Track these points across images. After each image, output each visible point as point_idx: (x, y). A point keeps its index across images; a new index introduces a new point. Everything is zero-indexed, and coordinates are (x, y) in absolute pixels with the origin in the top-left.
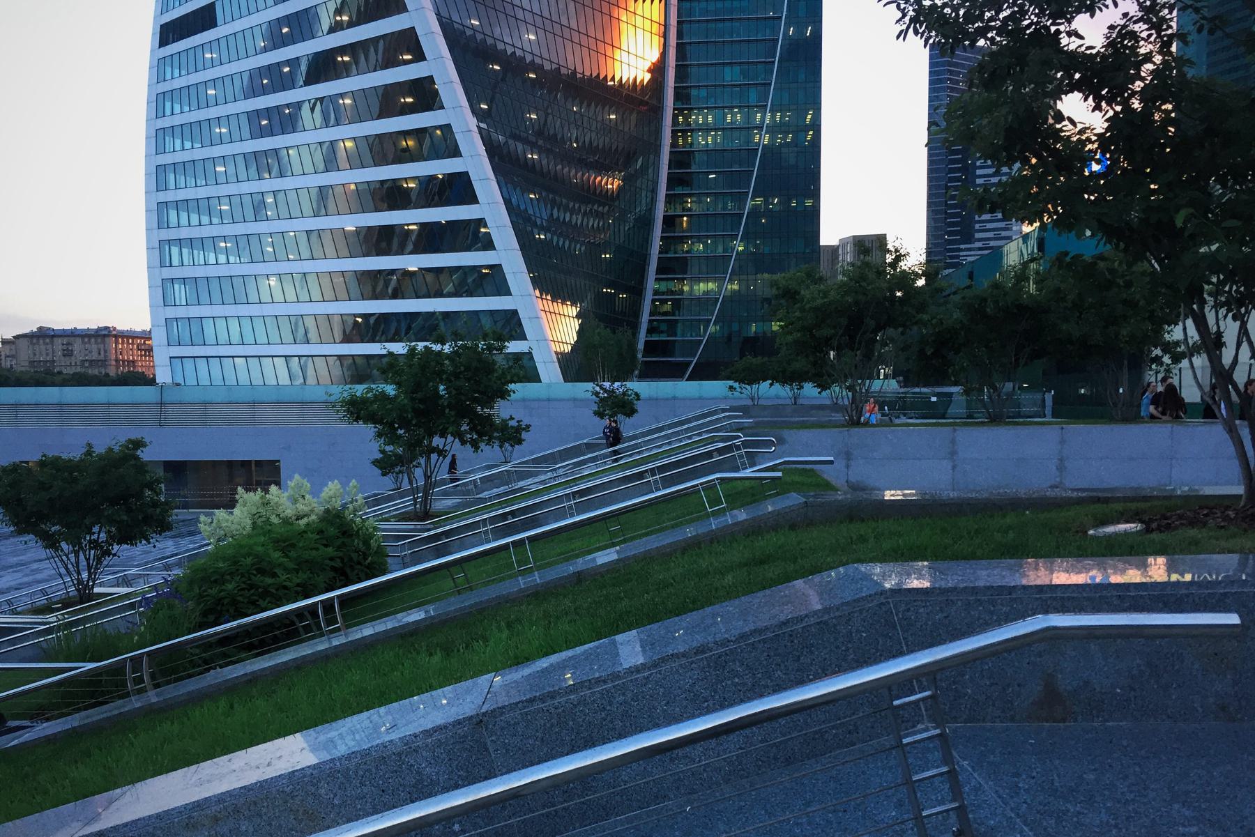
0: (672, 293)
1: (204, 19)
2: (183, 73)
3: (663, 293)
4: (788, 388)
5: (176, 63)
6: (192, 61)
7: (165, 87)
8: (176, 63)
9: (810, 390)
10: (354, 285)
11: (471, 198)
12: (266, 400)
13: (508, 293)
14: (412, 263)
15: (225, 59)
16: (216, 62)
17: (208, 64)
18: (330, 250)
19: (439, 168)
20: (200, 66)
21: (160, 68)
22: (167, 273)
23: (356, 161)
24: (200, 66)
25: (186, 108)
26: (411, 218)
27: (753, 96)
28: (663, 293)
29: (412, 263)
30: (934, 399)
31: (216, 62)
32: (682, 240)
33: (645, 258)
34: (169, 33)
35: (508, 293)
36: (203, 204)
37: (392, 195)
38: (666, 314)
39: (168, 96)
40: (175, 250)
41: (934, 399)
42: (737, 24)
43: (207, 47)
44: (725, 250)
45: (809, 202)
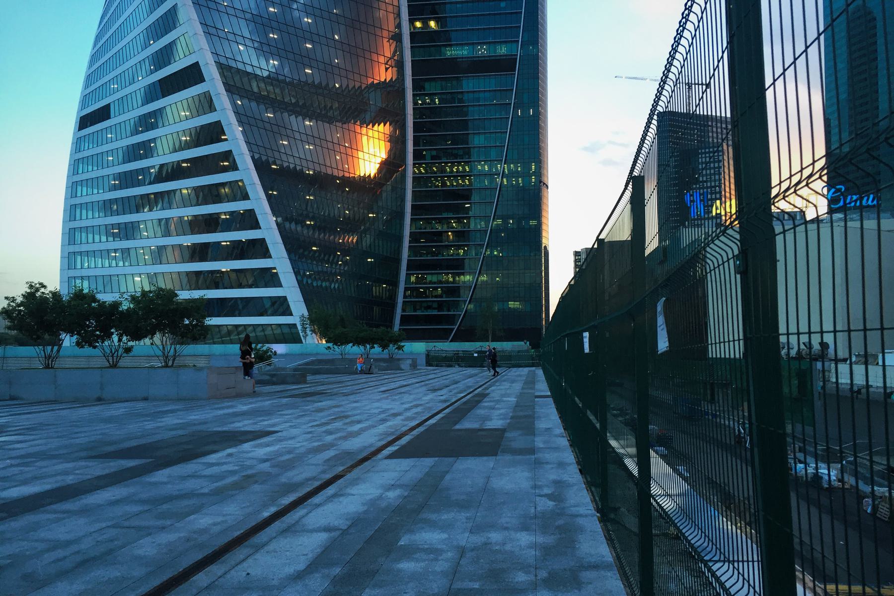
0: (440, 282)
1: (103, 114)
2: (91, 146)
3: (435, 283)
4: (362, 348)
5: (87, 140)
6: (97, 138)
7: (80, 155)
8: (87, 140)
9: (377, 349)
10: (185, 280)
11: (256, 225)
12: (142, 354)
13: (281, 286)
14: (225, 266)
15: (119, 137)
16: (114, 139)
17: (109, 140)
18: (171, 258)
19: (240, 206)
20: (104, 142)
21: (78, 145)
22: (72, 273)
23: (186, 203)
24: (104, 142)
25: (95, 168)
26: (224, 238)
27: (493, 154)
28: (435, 283)
29: (225, 266)
30: (476, 355)
31: (114, 139)
32: (448, 247)
33: (398, 261)
34: (85, 122)
35: (281, 286)
36: (103, 228)
37: (210, 223)
38: (436, 297)
39: (81, 161)
40: (79, 258)
41: (476, 355)
42: (483, 108)
43: (109, 130)
44: (476, 254)
45: (533, 223)
